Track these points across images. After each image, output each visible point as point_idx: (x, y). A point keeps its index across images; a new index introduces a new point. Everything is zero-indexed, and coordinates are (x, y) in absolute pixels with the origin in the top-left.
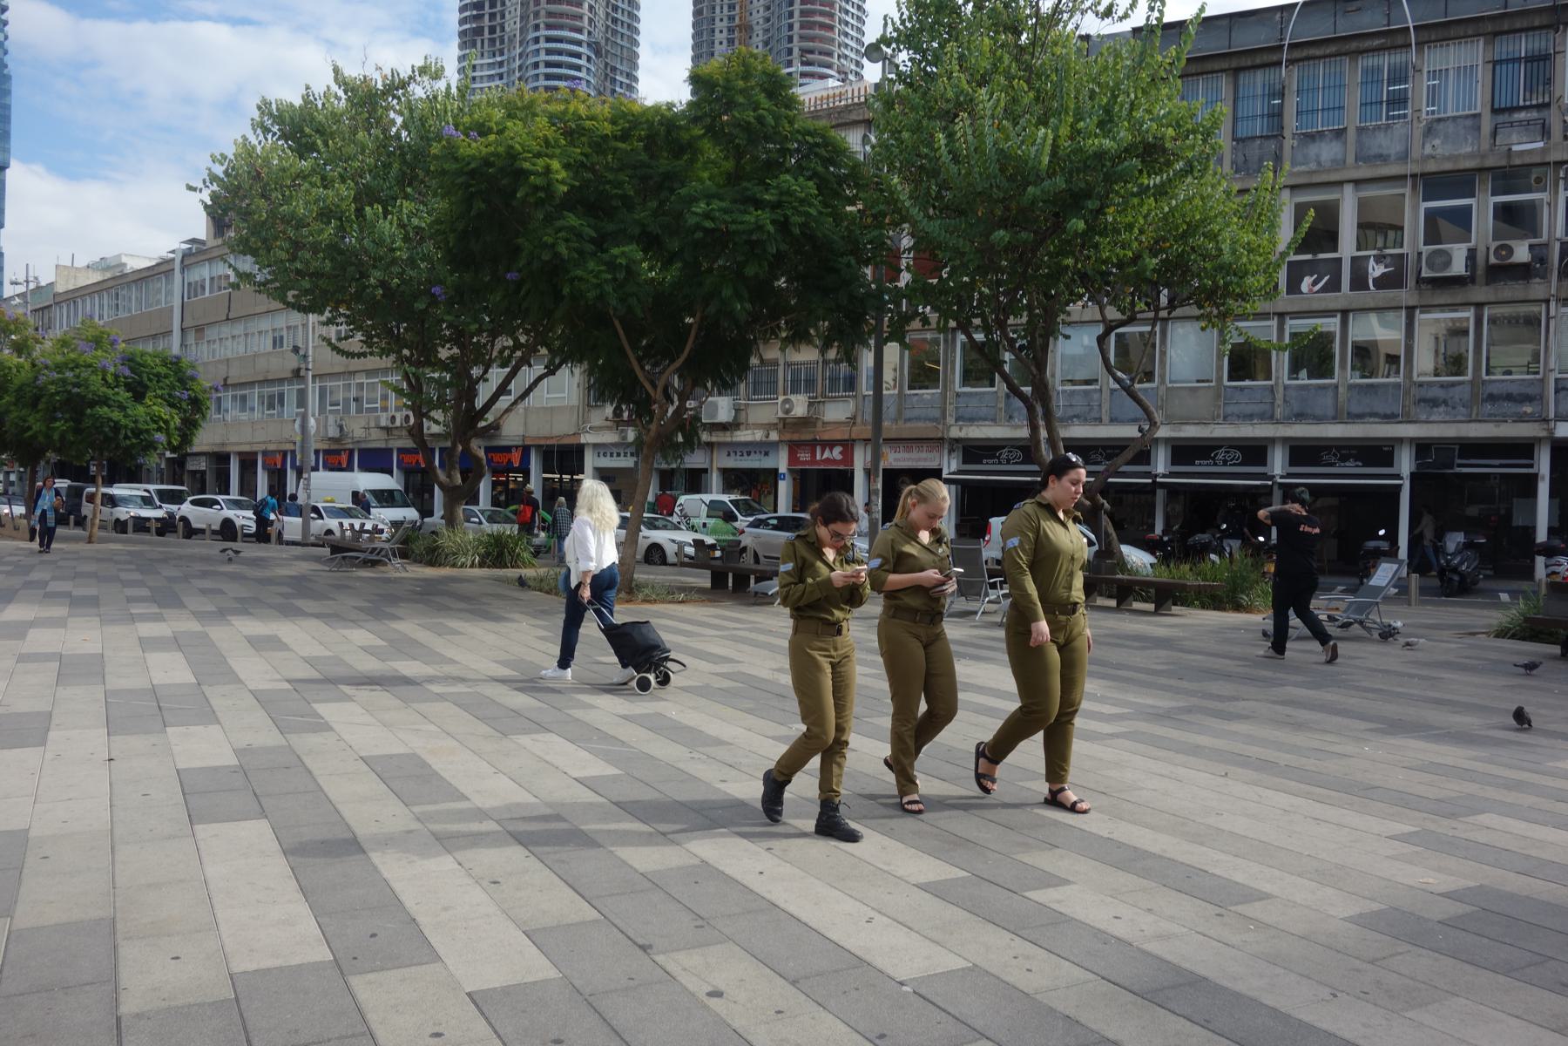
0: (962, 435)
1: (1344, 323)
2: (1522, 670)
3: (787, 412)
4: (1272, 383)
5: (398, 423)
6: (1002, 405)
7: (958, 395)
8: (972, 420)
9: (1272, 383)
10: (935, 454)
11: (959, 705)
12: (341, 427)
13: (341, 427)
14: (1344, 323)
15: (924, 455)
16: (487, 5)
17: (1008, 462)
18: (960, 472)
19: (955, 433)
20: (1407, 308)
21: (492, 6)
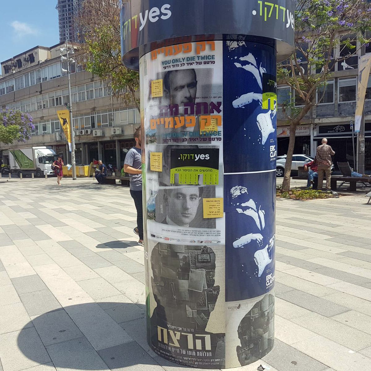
0: (320, 122)
1: (336, 82)
2: (147, 210)
3: (115, 133)
4: (333, 103)
5: (83, 134)
6: (337, 109)
7: (317, 106)
8: (323, 116)
9: (333, 103)
10: (307, 130)
11: (136, 222)
12: (61, 136)
13: (61, 136)
14: (336, 82)
15: (303, 131)
16: (67, 1)
17: (339, 131)
18: (318, 136)
19: (317, 121)
20: (335, 78)
21: (69, 1)
